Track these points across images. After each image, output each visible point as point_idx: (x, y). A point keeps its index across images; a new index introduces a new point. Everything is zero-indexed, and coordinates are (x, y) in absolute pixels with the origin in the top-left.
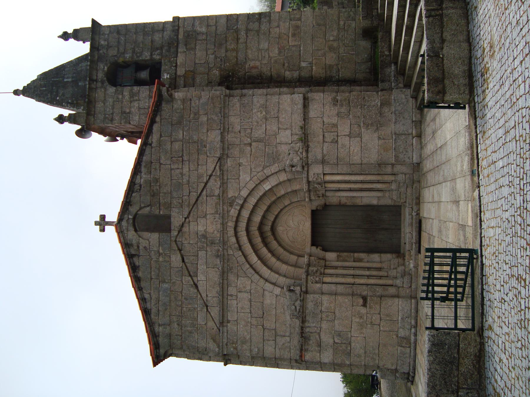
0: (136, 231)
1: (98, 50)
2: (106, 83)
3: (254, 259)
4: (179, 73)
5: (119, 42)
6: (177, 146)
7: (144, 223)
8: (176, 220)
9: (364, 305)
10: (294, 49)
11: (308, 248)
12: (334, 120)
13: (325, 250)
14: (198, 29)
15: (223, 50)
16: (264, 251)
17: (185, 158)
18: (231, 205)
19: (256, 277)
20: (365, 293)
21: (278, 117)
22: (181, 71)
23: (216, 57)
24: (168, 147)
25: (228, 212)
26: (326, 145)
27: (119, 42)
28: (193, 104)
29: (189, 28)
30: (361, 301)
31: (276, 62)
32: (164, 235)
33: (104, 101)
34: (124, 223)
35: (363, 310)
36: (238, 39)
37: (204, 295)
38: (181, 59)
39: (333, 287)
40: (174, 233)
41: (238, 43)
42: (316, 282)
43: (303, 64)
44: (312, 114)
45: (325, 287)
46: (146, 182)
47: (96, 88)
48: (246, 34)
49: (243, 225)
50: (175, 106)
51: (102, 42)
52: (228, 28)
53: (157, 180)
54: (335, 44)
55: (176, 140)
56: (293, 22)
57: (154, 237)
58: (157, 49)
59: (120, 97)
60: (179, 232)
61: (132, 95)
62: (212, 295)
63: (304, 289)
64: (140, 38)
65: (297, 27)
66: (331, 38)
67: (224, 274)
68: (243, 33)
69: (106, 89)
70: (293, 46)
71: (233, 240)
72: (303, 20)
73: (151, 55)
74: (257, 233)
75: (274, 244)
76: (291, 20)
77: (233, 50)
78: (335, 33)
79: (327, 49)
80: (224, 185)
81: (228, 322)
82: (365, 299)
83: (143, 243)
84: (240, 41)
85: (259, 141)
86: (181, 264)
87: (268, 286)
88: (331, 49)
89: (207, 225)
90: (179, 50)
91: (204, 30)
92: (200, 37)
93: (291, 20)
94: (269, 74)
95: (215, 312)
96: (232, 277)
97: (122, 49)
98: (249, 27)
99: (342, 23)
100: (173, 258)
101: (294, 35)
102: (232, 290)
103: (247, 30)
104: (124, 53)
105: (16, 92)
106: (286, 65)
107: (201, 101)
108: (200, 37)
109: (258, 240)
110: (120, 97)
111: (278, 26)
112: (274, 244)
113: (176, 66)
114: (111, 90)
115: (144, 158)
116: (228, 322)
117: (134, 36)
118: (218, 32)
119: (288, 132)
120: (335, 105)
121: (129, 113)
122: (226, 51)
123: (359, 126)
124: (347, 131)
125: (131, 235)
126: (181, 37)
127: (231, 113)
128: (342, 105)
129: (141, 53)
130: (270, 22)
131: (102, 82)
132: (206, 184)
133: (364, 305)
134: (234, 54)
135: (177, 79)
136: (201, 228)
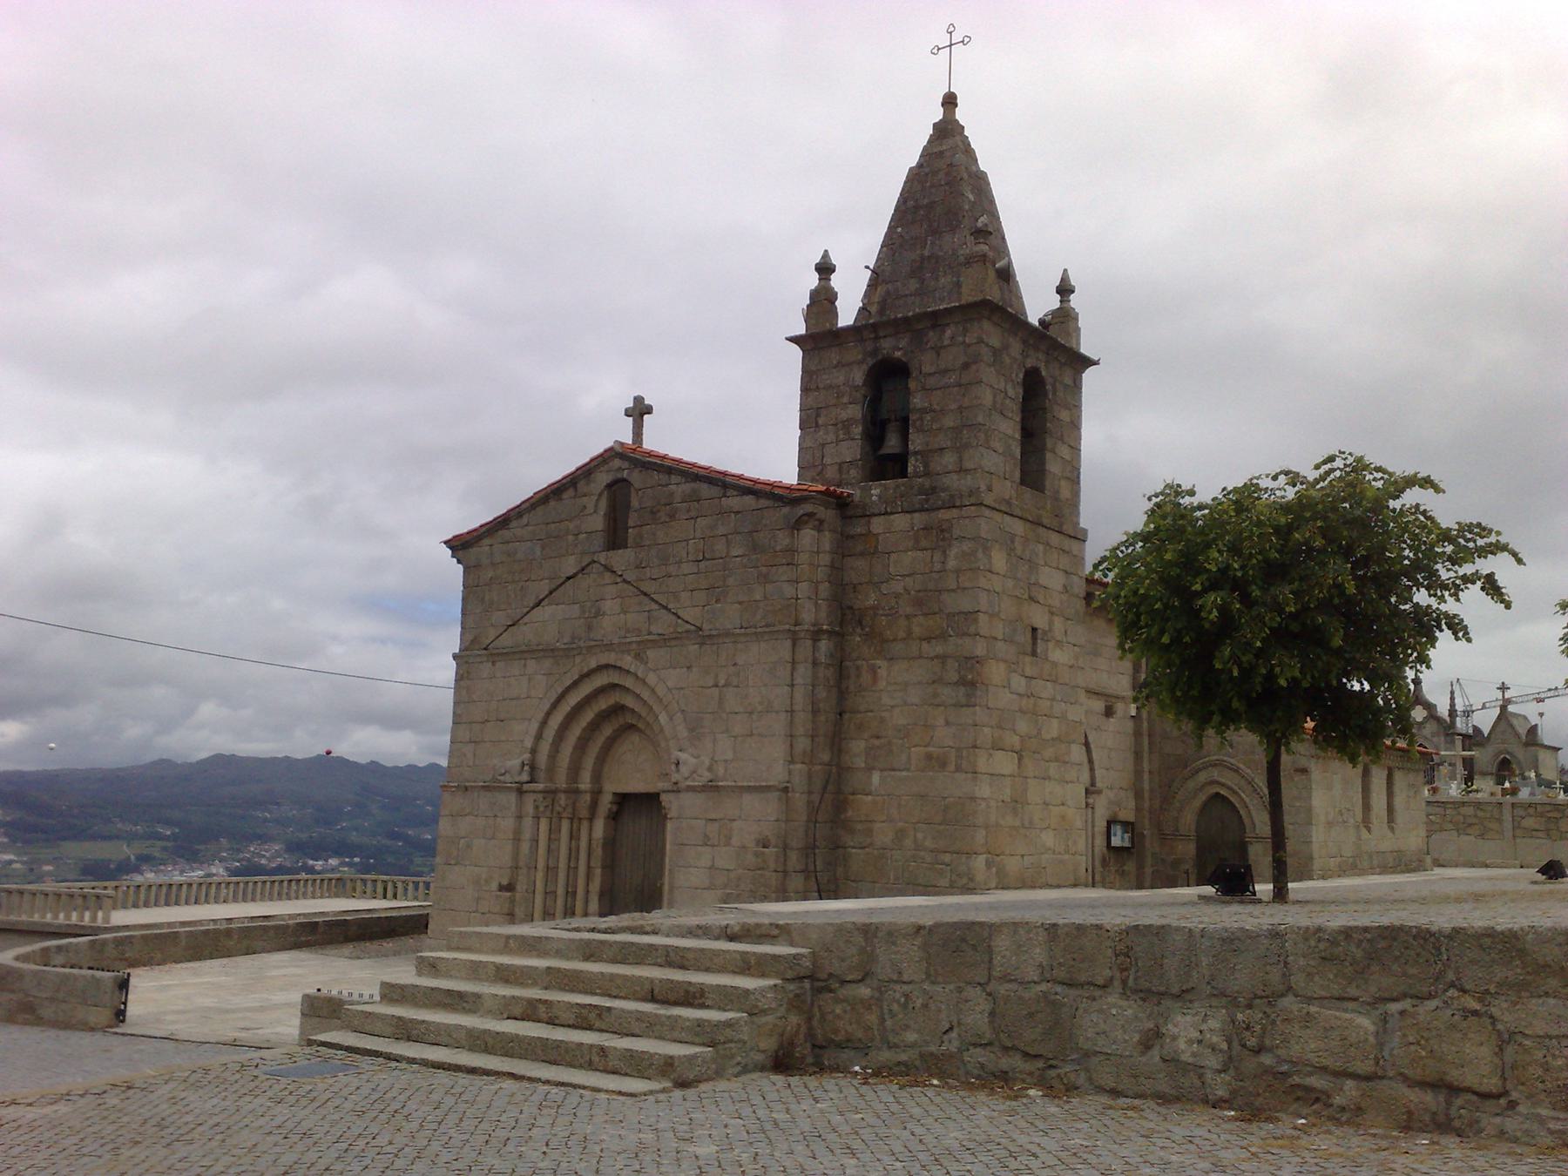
0: (609, 486)
1: (934, 327)
2: (871, 361)
3: (573, 699)
4: (875, 520)
5: (946, 371)
6: (720, 547)
7: (627, 498)
8: (621, 559)
9: (501, 888)
10: (904, 757)
11: (611, 787)
12: (735, 841)
13: (614, 817)
14: (953, 552)
15: (909, 610)
16: (589, 715)
17: (702, 565)
18: (638, 656)
19: (547, 707)
20: (518, 887)
21: (752, 735)
22: (877, 525)
23: (897, 596)
24: (721, 530)
25: (628, 652)
26: (701, 823)
27: (946, 371)
28: (781, 569)
29: (956, 532)
30: (505, 882)
31: (882, 720)
32: (599, 541)
33: (840, 365)
34: (617, 463)
35: (494, 886)
36: (928, 639)
37: (526, 619)
38: (900, 521)
39: (527, 835)
40: (602, 557)
41: (921, 639)
42: (537, 807)
43: (876, 778)
44: (747, 799)
45: (528, 822)
46: (672, 494)
47: (862, 340)
48: (937, 657)
49: (615, 678)
50: (780, 534)
51: (949, 333)
52: (950, 616)
53: (672, 516)
54: (908, 842)
55: (728, 543)
56: (953, 753)
57: (597, 522)
58: (926, 465)
59: (845, 400)
60: (605, 567)
61: (846, 425)
62: (525, 634)
63: (525, 787)
64: (949, 422)
65: (943, 765)
66: (920, 836)
67: (549, 652)
68: (939, 649)
69: (860, 363)
70: (909, 758)
71: (593, 665)
72: (957, 775)
73: (916, 453)
74: (611, 701)
75: (607, 730)
76: (959, 750)
77: (909, 633)
78: (928, 843)
79: (900, 824)
80: (663, 641)
81: (494, 663)
82: (510, 888)
83: (589, 502)
84: (925, 645)
85: (721, 700)
86: (564, 576)
87: (535, 726)
88: (900, 835)
89: (616, 617)
90: (916, 515)
91: (952, 563)
92: (938, 556)
93: (959, 750)
94: (862, 708)
95: (507, 640)
96: (547, 663)
97: (932, 382)
98: (950, 661)
99: (947, 858)
100: (572, 560)
101: (929, 757)
102: (531, 664)
103: (943, 658)
104: (924, 389)
105: (950, 101)
106: (877, 742)
107: (785, 585)
108: (938, 556)
109: (603, 704)
110: (845, 400)
111: (947, 723)
112: (607, 730)
113: (886, 513)
114: (859, 376)
115: (705, 486)
116: (494, 663)
117: (954, 406)
118: (945, 596)
119: (730, 755)
120: (758, 843)
121: (817, 425)
122: (908, 617)
123: (725, 887)
124: (720, 863)
125: (603, 478)
126: (943, 515)
127: (763, 645)
128: (756, 854)
129: (920, 430)
130: (958, 705)
131: (875, 352)
132: (665, 608)
133: (501, 888)
134: (902, 634)
135: (863, 521)
136: (608, 606)
